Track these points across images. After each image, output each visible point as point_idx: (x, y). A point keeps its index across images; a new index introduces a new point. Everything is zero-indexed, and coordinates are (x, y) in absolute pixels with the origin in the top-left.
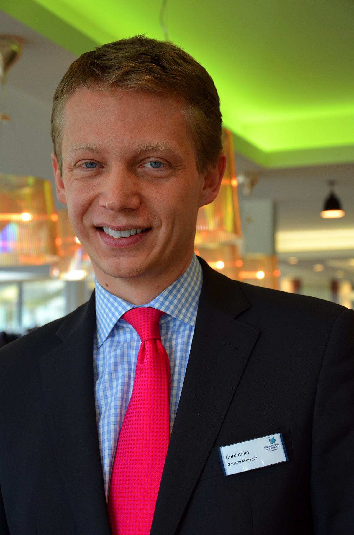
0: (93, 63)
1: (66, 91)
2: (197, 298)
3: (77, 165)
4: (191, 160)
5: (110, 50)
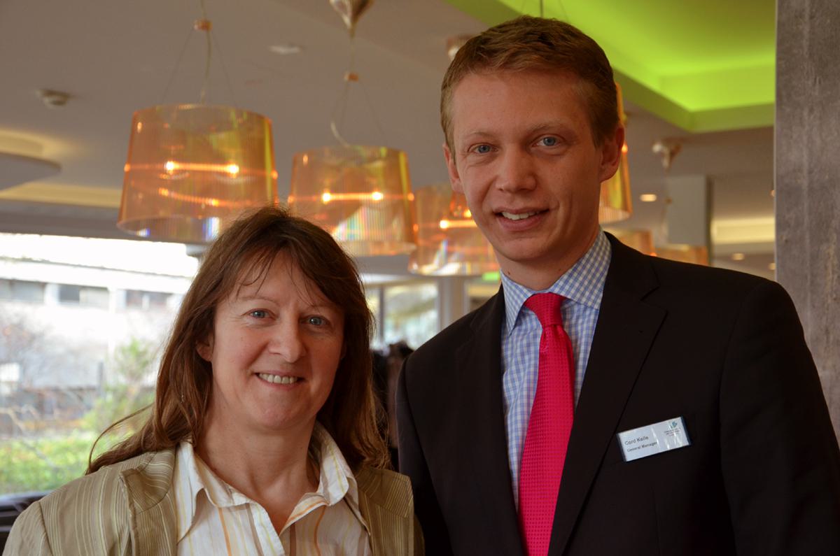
0: (479, 49)
1: (454, 79)
2: (603, 279)
3: (469, 150)
4: (587, 134)
5: (495, 33)
